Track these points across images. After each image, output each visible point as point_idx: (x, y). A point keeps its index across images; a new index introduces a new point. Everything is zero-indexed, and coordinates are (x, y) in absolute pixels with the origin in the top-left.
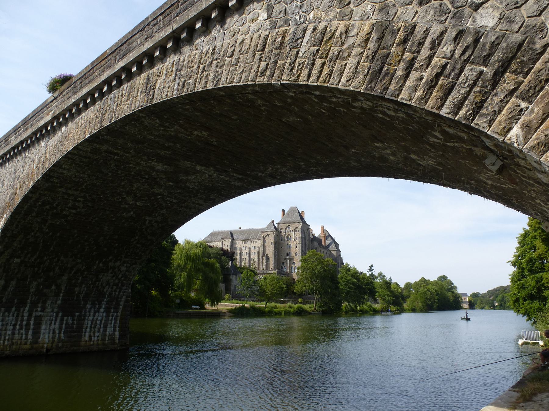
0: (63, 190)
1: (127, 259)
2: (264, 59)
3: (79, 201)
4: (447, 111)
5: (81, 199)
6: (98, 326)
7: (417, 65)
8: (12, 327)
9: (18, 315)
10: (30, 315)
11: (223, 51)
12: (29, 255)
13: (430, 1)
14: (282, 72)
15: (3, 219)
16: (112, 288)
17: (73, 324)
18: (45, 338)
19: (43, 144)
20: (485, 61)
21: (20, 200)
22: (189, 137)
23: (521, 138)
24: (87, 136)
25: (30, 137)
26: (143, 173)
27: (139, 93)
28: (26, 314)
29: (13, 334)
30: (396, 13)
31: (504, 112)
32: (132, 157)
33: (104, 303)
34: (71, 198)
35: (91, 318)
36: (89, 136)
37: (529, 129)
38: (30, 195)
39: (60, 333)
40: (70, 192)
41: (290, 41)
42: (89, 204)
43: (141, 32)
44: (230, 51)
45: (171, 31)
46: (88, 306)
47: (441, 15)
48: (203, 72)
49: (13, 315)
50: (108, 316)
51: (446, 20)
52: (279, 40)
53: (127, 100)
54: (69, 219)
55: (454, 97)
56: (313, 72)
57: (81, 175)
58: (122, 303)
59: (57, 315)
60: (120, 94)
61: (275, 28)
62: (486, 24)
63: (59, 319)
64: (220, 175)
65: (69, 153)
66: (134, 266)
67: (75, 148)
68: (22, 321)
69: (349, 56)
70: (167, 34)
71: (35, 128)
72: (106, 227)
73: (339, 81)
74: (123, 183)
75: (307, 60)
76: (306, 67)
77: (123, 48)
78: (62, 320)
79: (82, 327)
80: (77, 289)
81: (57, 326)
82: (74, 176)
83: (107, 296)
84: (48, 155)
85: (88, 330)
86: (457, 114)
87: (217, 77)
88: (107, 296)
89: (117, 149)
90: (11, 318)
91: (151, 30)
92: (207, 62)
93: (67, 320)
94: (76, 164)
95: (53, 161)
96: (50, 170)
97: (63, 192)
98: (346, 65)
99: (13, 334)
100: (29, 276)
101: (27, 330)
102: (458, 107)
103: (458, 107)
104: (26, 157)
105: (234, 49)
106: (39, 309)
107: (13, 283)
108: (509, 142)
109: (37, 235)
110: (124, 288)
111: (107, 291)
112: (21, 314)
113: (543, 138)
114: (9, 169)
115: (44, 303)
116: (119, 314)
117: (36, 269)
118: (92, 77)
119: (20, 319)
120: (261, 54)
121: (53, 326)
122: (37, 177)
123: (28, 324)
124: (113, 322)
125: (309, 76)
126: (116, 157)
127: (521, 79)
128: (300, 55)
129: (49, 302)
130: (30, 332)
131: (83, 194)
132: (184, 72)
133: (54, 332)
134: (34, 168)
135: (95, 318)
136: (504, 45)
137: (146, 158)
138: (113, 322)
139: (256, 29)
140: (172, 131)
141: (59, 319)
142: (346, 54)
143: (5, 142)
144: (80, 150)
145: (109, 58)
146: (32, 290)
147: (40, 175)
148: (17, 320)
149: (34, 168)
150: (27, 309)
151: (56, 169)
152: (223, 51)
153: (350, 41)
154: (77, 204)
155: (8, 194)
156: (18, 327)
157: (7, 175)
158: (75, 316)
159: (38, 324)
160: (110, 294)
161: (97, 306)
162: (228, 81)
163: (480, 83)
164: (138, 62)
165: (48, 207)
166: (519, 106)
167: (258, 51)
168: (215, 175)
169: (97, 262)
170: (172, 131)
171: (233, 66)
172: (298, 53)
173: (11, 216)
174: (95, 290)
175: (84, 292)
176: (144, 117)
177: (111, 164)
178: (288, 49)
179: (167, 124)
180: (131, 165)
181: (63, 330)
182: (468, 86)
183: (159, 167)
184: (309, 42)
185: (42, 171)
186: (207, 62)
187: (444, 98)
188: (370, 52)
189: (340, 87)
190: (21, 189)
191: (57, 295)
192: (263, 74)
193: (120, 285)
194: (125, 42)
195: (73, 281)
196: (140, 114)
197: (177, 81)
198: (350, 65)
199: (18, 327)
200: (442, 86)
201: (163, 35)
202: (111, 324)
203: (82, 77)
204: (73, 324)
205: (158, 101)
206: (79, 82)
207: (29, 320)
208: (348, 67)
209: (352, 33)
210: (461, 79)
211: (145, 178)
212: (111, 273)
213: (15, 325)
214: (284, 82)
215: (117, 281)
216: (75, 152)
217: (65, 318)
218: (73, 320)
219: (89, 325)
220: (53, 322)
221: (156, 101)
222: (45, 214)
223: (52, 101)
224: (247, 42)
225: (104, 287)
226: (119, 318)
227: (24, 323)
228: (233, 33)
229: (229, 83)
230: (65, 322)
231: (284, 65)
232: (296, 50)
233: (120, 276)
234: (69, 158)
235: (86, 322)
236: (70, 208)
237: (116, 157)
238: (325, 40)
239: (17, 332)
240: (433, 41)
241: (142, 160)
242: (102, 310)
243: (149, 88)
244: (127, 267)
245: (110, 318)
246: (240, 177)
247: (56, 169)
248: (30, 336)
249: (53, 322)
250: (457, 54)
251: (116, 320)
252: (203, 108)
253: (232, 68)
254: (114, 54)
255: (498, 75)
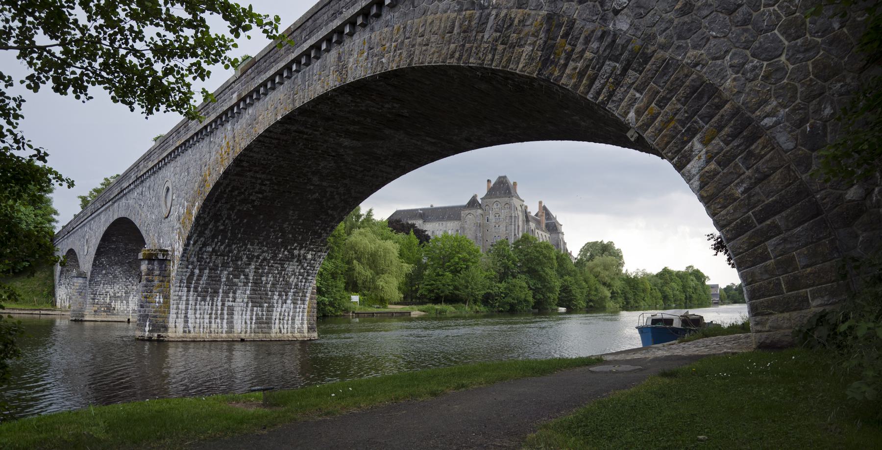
0: (251, 174)
1: (312, 246)
2: (453, 41)
3: (265, 185)
4: (592, 96)
5: (268, 183)
6: (286, 318)
7: (574, 56)
8: (208, 316)
9: (212, 305)
10: (223, 305)
11: (414, 30)
12: (219, 243)
13: (587, 1)
14: (469, 56)
15: (196, 207)
16: (298, 278)
17: (263, 315)
18: (238, 326)
19: (229, 126)
20: (616, 59)
21: (211, 187)
22: (380, 111)
23: (634, 120)
24: (279, 118)
25: (215, 121)
26: (330, 150)
27: (331, 72)
28: (219, 304)
29: (210, 323)
30: (562, 8)
31: (626, 100)
32: (321, 134)
33: (290, 294)
34: (259, 181)
35: (279, 310)
36: (281, 117)
37: (639, 113)
38: (221, 181)
39: (251, 323)
40: (258, 176)
41: (476, 25)
42: (276, 187)
43: (327, 7)
44: (421, 30)
45: (360, 8)
46: (276, 297)
47: (593, 16)
48: (395, 50)
49: (209, 305)
50: (295, 308)
51: (597, 19)
52: (466, 23)
53: (319, 79)
54: (256, 204)
55: (597, 85)
56: (496, 57)
57: (270, 157)
58: (308, 295)
59: (247, 306)
60: (311, 73)
61: (462, 11)
62: (622, 28)
63: (249, 309)
64: (411, 139)
65: (261, 135)
66: (319, 254)
67: (265, 131)
68: (217, 310)
69: (525, 44)
70: (356, 11)
71: (220, 111)
72: (291, 212)
73: (517, 67)
74: (310, 163)
75: (491, 45)
76: (490, 52)
77: (308, 24)
78: (252, 310)
79: (271, 319)
80: (264, 279)
81: (248, 317)
82: (262, 159)
83: (293, 287)
84: (237, 140)
85: (277, 321)
86: (597, 99)
87: (411, 55)
88: (293, 287)
89: (306, 128)
90: (207, 307)
91: (338, 4)
92: (399, 41)
93: (257, 311)
94: (265, 147)
95: (244, 144)
96: (241, 155)
97: (251, 176)
98: (522, 52)
99: (210, 323)
100: (220, 265)
101: (222, 319)
102: (598, 93)
103: (598, 93)
104: (211, 142)
105: (425, 29)
106: (231, 299)
107: (207, 271)
108: (627, 122)
109: (226, 222)
110: (310, 278)
111: (293, 282)
112: (215, 303)
113: (646, 120)
114: (193, 156)
115: (234, 293)
116: (306, 306)
117: (226, 258)
118: (277, 56)
119: (214, 308)
120: (451, 36)
121: (244, 317)
122: (227, 163)
123: (222, 314)
124: (301, 314)
125: (492, 60)
126: (305, 136)
127: (638, 75)
128: (485, 40)
129: (239, 292)
130: (225, 321)
131: (269, 177)
132: (376, 51)
133: (246, 323)
134: (223, 153)
135: (283, 309)
136: (630, 47)
137: (334, 134)
138: (301, 314)
139: (444, 9)
140: (362, 106)
141: (249, 309)
142: (522, 42)
143: (185, 127)
144: (271, 132)
145: (295, 34)
146: (224, 279)
147: (231, 161)
148: (212, 309)
149: (223, 153)
150: (220, 299)
151: (246, 152)
152: (414, 30)
153: (526, 29)
154: (263, 188)
155: (196, 182)
156: (213, 316)
157: (192, 162)
158: (263, 307)
159: (231, 312)
160: (296, 285)
161: (284, 297)
162: (420, 61)
163: (613, 76)
164: (328, 39)
165: (236, 193)
166: (635, 96)
167: (447, 33)
168: (406, 139)
169: (283, 250)
170: (362, 106)
171: (424, 45)
172: (483, 37)
173: (203, 204)
174: (281, 279)
175: (270, 283)
176: (337, 95)
177: (299, 144)
178: (474, 33)
179: (359, 100)
180: (319, 144)
181: (254, 321)
182: (606, 78)
183: (346, 142)
184: (493, 28)
185: (233, 156)
186: (399, 41)
187: (590, 86)
188: (542, 42)
189: (517, 72)
190: (211, 176)
191: (246, 284)
192: (452, 56)
193: (306, 274)
194: (311, 18)
195: (260, 271)
196: (334, 93)
197: (371, 60)
198: (527, 52)
199: (213, 316)
200: (589, 76)
201: (352, 13)
202: (299, 316)
203: (266, 55)
204: (263, 315)
205: (352, 81)
206: (262, 61)
207: (222, 310)
208: (524, 55)
209: (528, 23)
210: (602, 71)
211: (332, 156)
212: (297, 262)
213: (211, 314)
214: (472, 65)
215: (302, 271)
216: (267, 134)
217: (255, 309)
218: (262, 311)
219: (278, 317)
220: (244, 312)
221: (350, 80)
222: (234, 200)
223: (234, 82)
224: (437, 22)
225: (290, 278)
226: (306, 311)
227: (219, 312)
228: (423, 11)
229: (422, 63)
230: (255, 313)
231: (471, 48)
232: (481, 34)
233: (306, 265)
234: (260, 141)
235: (274, 313)
236: (256, 193)
237: (305, 136)
238: (505, 26)
239: (213, 321)
240: (586, 37)
241: (331, 137)
242: (289, 302)
243: (342, 68)
244: (312, 255)
245: (298, 310)
246: (433, 141)
247: (246, 152)
248: (225, 325)
249: (244, 312)
250: (601, 49)
251: (303, 312)
252: (396, 83)
253: (424, 48)
254: (299, 30)
255: (625, 70)
